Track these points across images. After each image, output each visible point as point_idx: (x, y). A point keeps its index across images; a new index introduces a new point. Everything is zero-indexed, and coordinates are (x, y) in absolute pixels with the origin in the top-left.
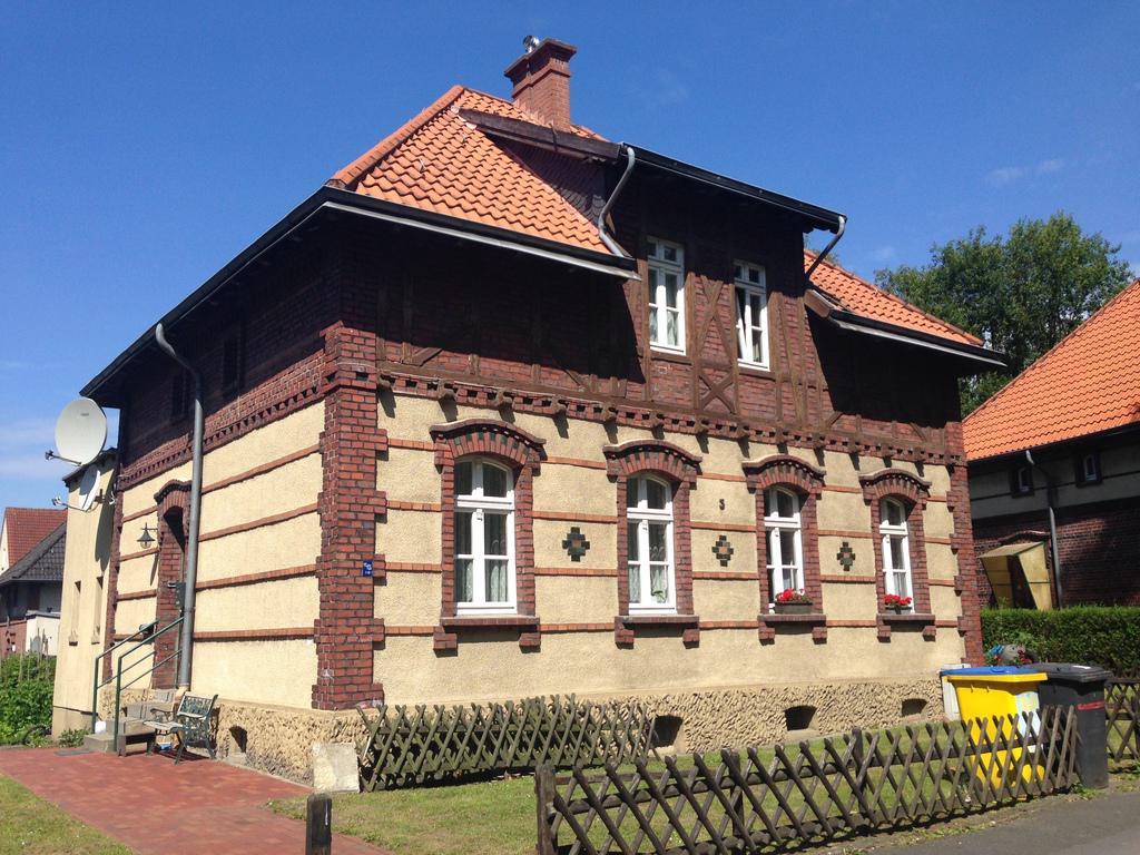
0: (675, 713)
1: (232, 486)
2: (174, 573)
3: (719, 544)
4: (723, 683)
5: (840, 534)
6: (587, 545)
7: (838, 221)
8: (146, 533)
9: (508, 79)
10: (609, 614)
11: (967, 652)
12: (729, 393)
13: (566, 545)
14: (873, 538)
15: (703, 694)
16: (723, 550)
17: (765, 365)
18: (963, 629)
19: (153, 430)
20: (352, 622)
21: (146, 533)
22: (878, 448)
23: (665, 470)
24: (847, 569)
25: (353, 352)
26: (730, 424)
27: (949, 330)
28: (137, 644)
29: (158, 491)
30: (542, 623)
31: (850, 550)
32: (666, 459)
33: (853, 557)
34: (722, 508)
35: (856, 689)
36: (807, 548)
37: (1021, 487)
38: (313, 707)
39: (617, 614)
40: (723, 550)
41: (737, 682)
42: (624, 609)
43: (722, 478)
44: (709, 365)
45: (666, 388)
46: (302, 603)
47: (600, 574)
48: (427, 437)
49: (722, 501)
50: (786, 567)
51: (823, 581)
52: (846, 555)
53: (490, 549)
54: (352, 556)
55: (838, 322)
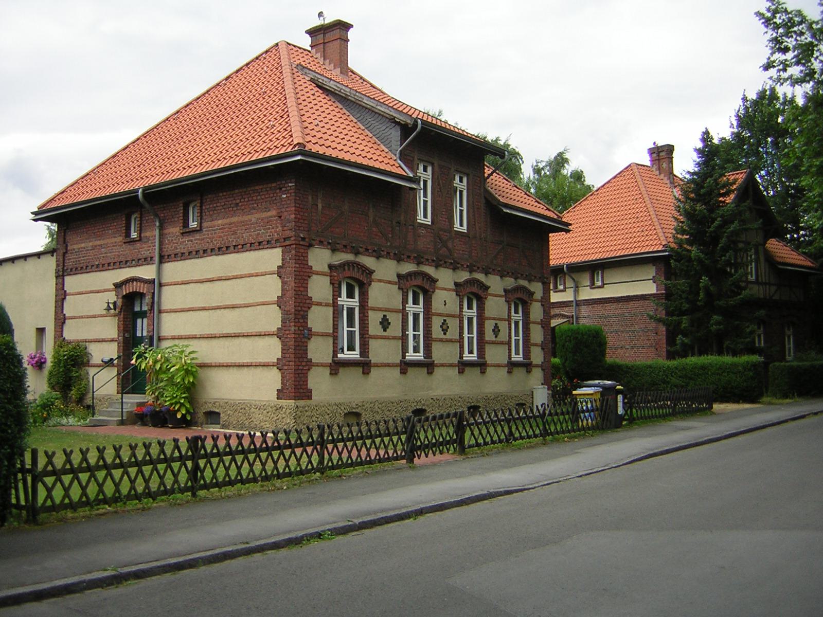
0: (424, 407)
1: (192, 285)
2: (128, 329)
3: (443, 324)
4: (442, 393)
5: (494, 319)
6: (389, 324)
7: (504, 154)
8: (108, 306)
9: (308, 36)
10: (397, 359)
11: (544, 380)
12: (450, 244)
13: (381, 323)
14: (331, 276)
15: (435, 398)
16: (445, 327)
17: (464, 229)
18: (543, 368)
19: (98, 243)
20: (301, 360)
21: (108, 306)
22: (513, 273)
23: (422, 285)
24: (496, 337)
25: (300, 227)
26: (450, 261)
27: (547, 209)
28: (101, 368)
29: (118, 281)
30: (372, 362)
31: (498, 327)
32: (423, 280)
33: (499, 330)
34: (445, 305)
35: (498, 397)
36: (525, 335)
37: (558, 286)
38: (278, 399)
39: (401, 358)
40: (445, 327)
41: (448, 393)
42: (404, 356)
43: (445, 289)
44: (442, 230)
45: (424, 243)
46: (272, 349)
47: (394, 338)
48: (326, 269)
49: (445, 301)
50: (470, 335)
51: (487, 343)
52: (496, 330)
53: (414, 330)
54: (300, 328)
55: (501, 207)
